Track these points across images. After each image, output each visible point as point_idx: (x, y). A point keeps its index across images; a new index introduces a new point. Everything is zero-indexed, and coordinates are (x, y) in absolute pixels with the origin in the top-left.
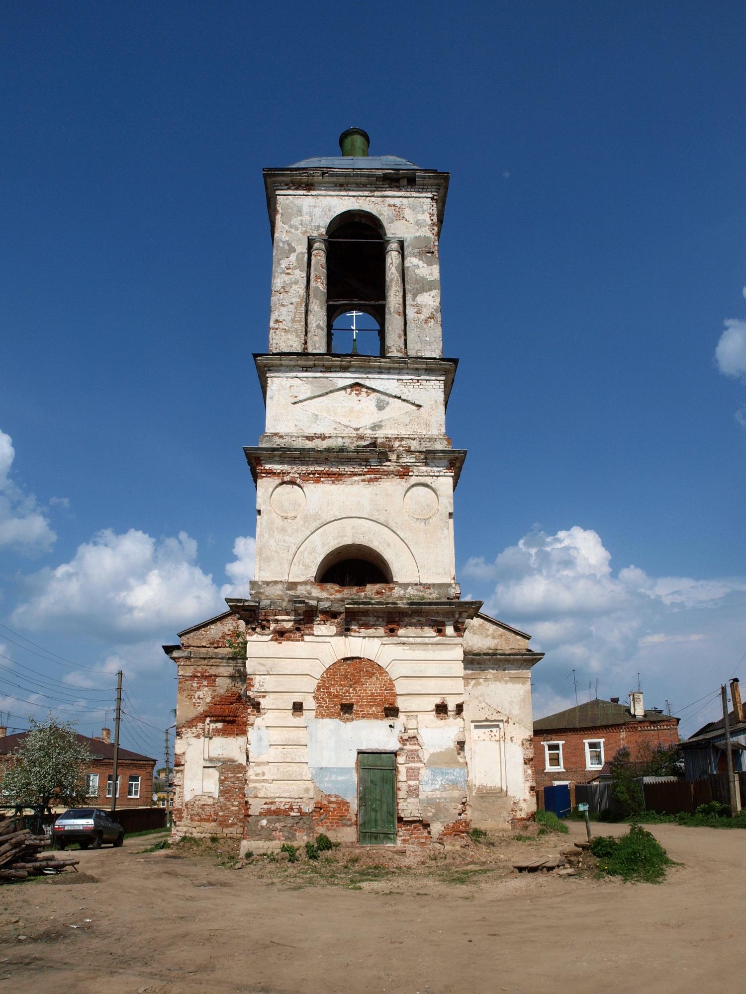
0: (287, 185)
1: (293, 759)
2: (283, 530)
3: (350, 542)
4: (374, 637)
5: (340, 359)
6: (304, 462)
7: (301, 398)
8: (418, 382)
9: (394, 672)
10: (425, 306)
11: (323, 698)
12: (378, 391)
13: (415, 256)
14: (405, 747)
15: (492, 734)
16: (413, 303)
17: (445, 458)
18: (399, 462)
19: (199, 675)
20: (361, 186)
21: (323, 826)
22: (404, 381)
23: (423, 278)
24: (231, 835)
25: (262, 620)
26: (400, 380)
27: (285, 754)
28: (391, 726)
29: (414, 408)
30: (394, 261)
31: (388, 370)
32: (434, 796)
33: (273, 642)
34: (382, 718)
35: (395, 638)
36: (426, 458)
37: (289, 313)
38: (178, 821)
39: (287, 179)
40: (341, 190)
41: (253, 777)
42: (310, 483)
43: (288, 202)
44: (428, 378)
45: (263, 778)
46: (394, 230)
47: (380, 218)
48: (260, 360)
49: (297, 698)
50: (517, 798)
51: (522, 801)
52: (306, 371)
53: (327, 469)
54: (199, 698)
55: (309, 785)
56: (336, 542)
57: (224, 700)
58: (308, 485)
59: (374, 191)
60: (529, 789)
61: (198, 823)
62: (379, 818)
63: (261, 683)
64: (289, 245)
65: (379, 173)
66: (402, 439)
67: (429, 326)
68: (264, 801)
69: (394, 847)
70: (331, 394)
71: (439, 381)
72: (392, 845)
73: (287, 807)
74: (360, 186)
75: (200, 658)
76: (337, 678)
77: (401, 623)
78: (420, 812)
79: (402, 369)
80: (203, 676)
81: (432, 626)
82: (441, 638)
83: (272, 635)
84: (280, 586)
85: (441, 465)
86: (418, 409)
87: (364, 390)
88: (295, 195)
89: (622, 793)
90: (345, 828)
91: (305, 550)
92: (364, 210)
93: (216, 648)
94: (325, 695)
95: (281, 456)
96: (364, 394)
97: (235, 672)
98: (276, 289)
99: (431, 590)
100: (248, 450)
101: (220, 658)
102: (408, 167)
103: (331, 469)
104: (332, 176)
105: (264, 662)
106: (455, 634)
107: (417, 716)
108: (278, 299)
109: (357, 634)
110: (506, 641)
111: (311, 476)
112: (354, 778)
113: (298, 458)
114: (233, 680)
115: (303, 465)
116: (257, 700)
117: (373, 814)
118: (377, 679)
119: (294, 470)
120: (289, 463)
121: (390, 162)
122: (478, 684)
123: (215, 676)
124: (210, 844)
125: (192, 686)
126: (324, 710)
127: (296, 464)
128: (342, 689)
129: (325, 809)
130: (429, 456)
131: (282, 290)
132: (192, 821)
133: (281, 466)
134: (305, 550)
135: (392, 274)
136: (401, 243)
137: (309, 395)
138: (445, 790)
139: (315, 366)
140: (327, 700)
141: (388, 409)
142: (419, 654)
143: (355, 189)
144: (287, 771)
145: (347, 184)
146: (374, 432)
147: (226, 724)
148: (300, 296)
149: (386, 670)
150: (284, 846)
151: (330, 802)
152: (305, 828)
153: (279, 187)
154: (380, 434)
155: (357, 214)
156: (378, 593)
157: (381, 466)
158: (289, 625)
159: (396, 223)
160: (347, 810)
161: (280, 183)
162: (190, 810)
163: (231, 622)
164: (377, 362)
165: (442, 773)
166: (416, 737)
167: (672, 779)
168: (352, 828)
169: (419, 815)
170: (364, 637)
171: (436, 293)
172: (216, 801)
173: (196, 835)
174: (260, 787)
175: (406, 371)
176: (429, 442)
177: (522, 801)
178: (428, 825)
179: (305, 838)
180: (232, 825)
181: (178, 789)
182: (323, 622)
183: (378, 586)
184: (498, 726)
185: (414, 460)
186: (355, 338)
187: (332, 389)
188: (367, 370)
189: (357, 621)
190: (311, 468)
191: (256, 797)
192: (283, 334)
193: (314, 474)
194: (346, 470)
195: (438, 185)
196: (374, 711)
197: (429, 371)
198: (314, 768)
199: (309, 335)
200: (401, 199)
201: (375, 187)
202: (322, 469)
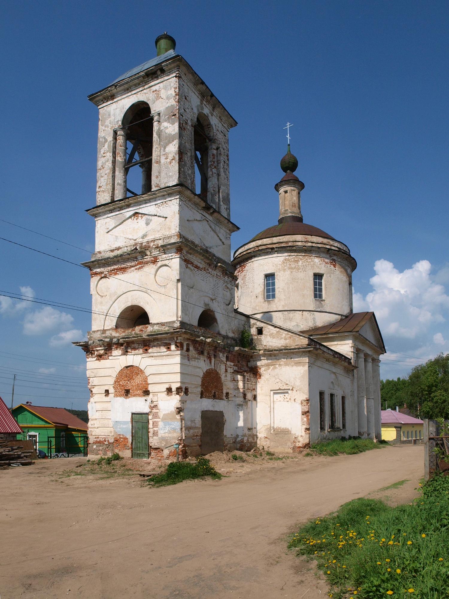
0: (102, 101)
3: (130, 305)
4: (138, 354)
6: (109, 265)
7: (110, 229)
9: (147, 372)
12: (146, 215)
14: (153, 411)
15: (285, 397)
17: (173, 248)
22: (158, 205)
23: (170, 134)
28: (146, 400)
32: (165, 436)
36: (164, 250)
39: (101, 98)
40: (128, 93)
44: (170, 199)
45: (94, 426)
50: (297, 435)
51: (299, 437)
52: (112, 212)
53: (119, 267)
55: (112, 429)
56: (124, 305)
59: (145, 85)
60: (304, 430)
62: (141, 446)
64: (105, 138)
67: (172, 165)
68: (95, 437)
73: (103, 440)
79: (156, 198)
81: (165, 346)
82: (169, 352)
84: (99, 333)
85: (173, 252)
87: (140, 215)
88: (107, 106)
98: (99, 168)
103: (122, 266)
104: (120, 86)
109: (130, 354)
110: (293, 340)
111: (113, 272)
115: (109, 266)
117: (139, 444)
118: (140, 376)
120: (103, 267)
122: (275, 368)
126: (118, 393)
127: (106, 267)
133: (99, 269)
139: (115, 209)
141: (151, 224)
145: (130, 88)
146: (143, 240)
157: (144, 259)
158: (102, 352)
161: (98, 101)
164: (141, 198)
165: (169, 424)
174: (93, 430)
175: (158, 198)
176: (168, 239)
177: (299, 437)
184: (287, 393)
185: (158, 252)
186: (289, 143)
187: (124, 219)
188: (139, 203)
190: (112, 268)
191: (92, 435)
192: (102, 193)
193: (114, 270)
196: (138, 393)
197: (170, 195)
201: (145, 83)
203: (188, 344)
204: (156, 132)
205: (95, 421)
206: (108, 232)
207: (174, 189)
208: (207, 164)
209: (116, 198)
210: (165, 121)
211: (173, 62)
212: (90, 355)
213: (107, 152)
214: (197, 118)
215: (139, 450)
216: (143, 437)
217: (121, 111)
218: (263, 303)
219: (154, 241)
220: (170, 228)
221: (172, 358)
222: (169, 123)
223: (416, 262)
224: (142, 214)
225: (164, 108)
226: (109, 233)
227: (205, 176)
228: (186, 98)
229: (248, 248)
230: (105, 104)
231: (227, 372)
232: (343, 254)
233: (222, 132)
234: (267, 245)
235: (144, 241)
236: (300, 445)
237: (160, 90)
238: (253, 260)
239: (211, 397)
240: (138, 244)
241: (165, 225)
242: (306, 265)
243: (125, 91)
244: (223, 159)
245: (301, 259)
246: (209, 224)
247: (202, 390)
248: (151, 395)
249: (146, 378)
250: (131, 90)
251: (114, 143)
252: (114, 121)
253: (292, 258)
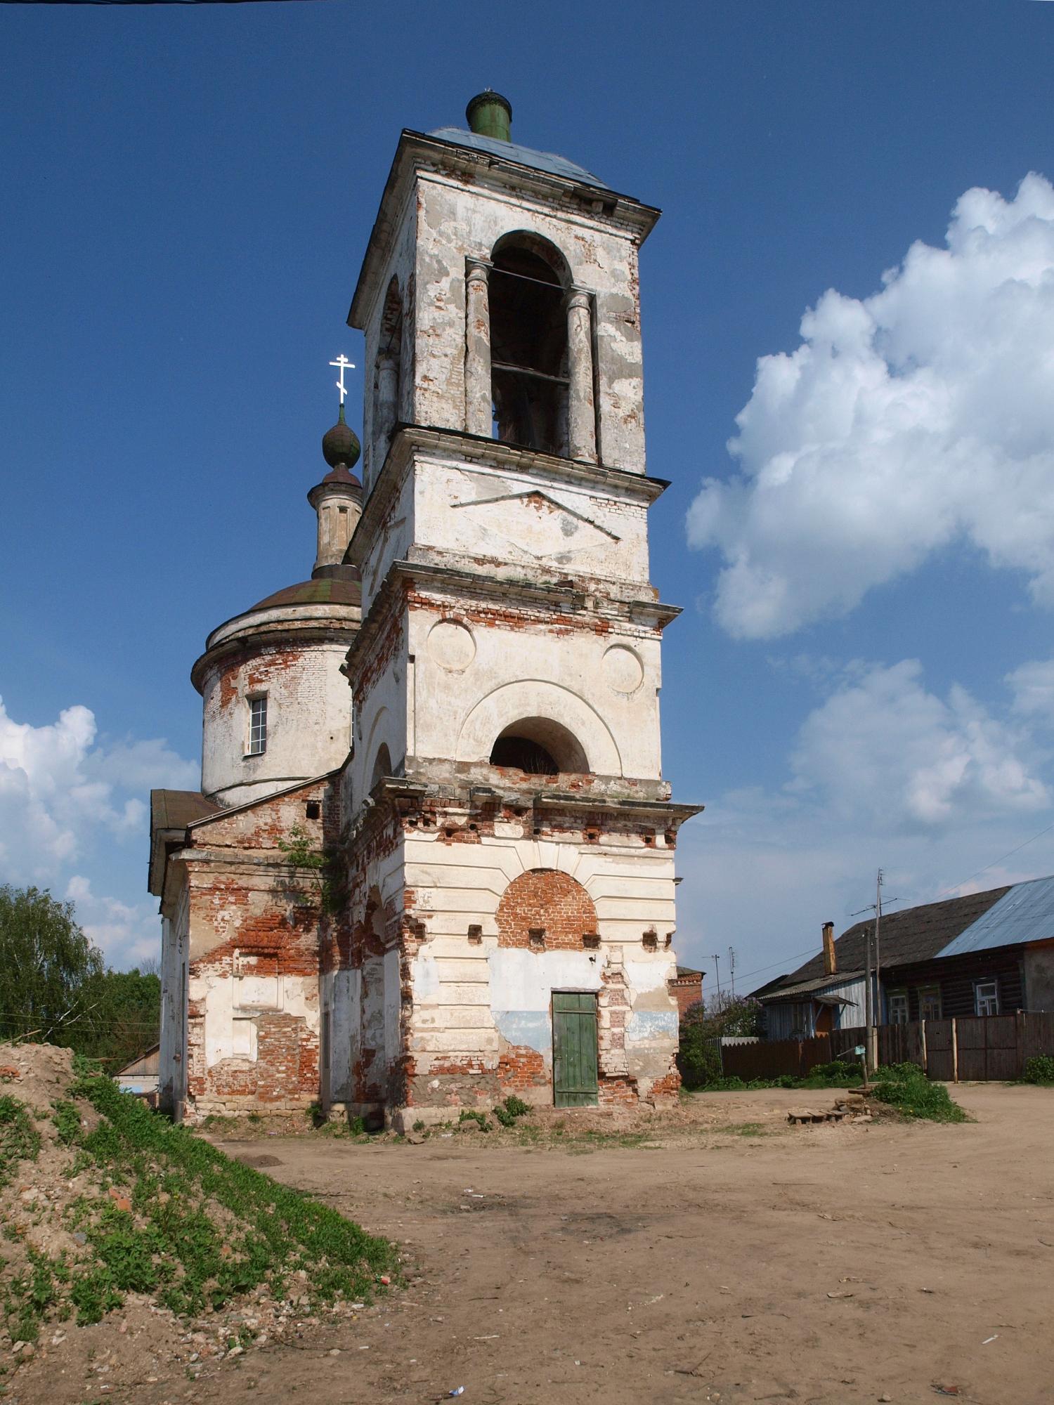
0: (434, 165)
1: (470, 1000)
2: (447, 688)
3: (534, 714)
5: (520, 453)
8: (615, 505)
9: (595, 889)
10: (625, 398)
11: (507, 921)
12: (565, 509)
13: (611, 322)
14: (608, 986)
16: (608, 390)
17: (653, 615)
18: (597, 613)
19: (223, 886)
20: (540, 197)
21: (510, 1086)
23: (621, 358)
24: (278, 1112)
25: (426, 812)
26: (593, 497)
27: (460, 994)
28: (591, 959)
29: (609, 539)
30: (583, 323)
31: (570, 480)
32: (643, 1046)
33: (439, 843)
34: (580, 949)
35: (595, 846)
36: (630, 612)
37: (443, 370)
38: (199, 1095)
39: (436, 156)
40: (511, 196)
41: (419, 1025)
42: (481, 626)
43: (434, 192)
45: (432, 1026)
46: (585, 276)
47: (565, 253)
48: (409, 433)
52: (471, 462)
53: (504, 609)
54: (223, 920)
56: (516, 712)
57: (260, 925)
58: (479, 628)
59: (557, 209)
61: (229, 1097)
62: (578, 1074)
63: (426, 898)
65: (570, 184)
66: (598, 581)
68: (434, 1055)
69: (598, 1109)
70: (502, 502)
71: (642, 507)
72: (595, 1107)
73: (465, 1062)
74: (539, 197)
75: (225, 862)
76: (525, 895)
77: (603, 827)
78: (626, 1065)
79: (596, 482)
80: (227, 889)
82: (649, 849)
83: (438, 834)
84: (447, 766)
86: (616, 543)
87: (546, 503)
88: (445, 185)
89: (696, 1056)
90: (538, 1088)
91: (477, 719)
92: (543, 234)
93: (245, 848)
94: (509, 916)
95: (443, 581)
96: (545, 509)
97: (277, 885)
98: (423, 329)
99: (638, 788)
100: (400, 566)
101: (255, 864)
102: (588, 181)
103: (510, 610)
104: (503, 170)
105: (428, 870)
106: (667, 846)
108: (427, 345)
109: (549, 838)
113: (467, 588)
114: (274, 897)
116: (420, 921)
117: (571, 1069)
118: (574, 898)
119: (460, 605)
120: (453, 593)
121: (555, 164)
123: (246, 889)
124: (249, 1124)
125: (212, 902)
127: (462, 596)
128: (531, 910)
129: (512, 1065)
130: (638, 610)
131: (431, 331)
132: (219, 1094)
133: (442, 596)
134: (477, 719)
135: (581, 341)
136: (592, 299)
137: (473, 498)
138: (655, 1038)
139: (483, 456)
140: (513, 923)
141: (576, 535)
142: (624, 868)
143: (533, 199)
144: (463, 1017)
145: (521, 189)
146: (561, 566)
147: (262, 958)
148: (457, 346)
149: (585, 887)
150: (463, 1113)
151: (518, 1056)
152: (488, 1089)
153: (422, 166)
154: (571, 569)
155: (529, 237)
156: (573, 786)
157: (574, 614)
158: (462, 821)
159: (585, 266)
160: (540, 1065)
161: (426, 159)
162: (215, 1079)
163: (269, 812)
164: (568, 467)
166: (620, 974)
167: (754, 1039)
168: (547, 1087)
169: (624, 1070)
170: (558, 843)
171: (637, 381)
172: (254, 1066)
173: (227, 1114)
174: (429, 1038)
178: (634, 1082)
179: (489, 1101)
180: (278, 1098)
181: (196, 1049)
182: (506, 820)
183: (573, 777)
185: (616, 613)
186: (342, 402)
187: (505, 494)
189: (550, 820)
190: (483, 605)
191: (424, 1051)
192: (435, 399)
193: (486, 613)
194: (529, 613)
195: (642, 224)
196: (570, 940)
197: (630, 492)
198: (498, 1012)
199: (471, 409)
200: (592, 231)
202: (498, 608)
207: (648, 486)
211: (641, 212)
215: (574, 1085)
216: (584, 1051)
221: (657, 865)
223: (70, 706)
229: (308, 614)
238: (325, 647)
241: (616, 554)
243: (505, 187)
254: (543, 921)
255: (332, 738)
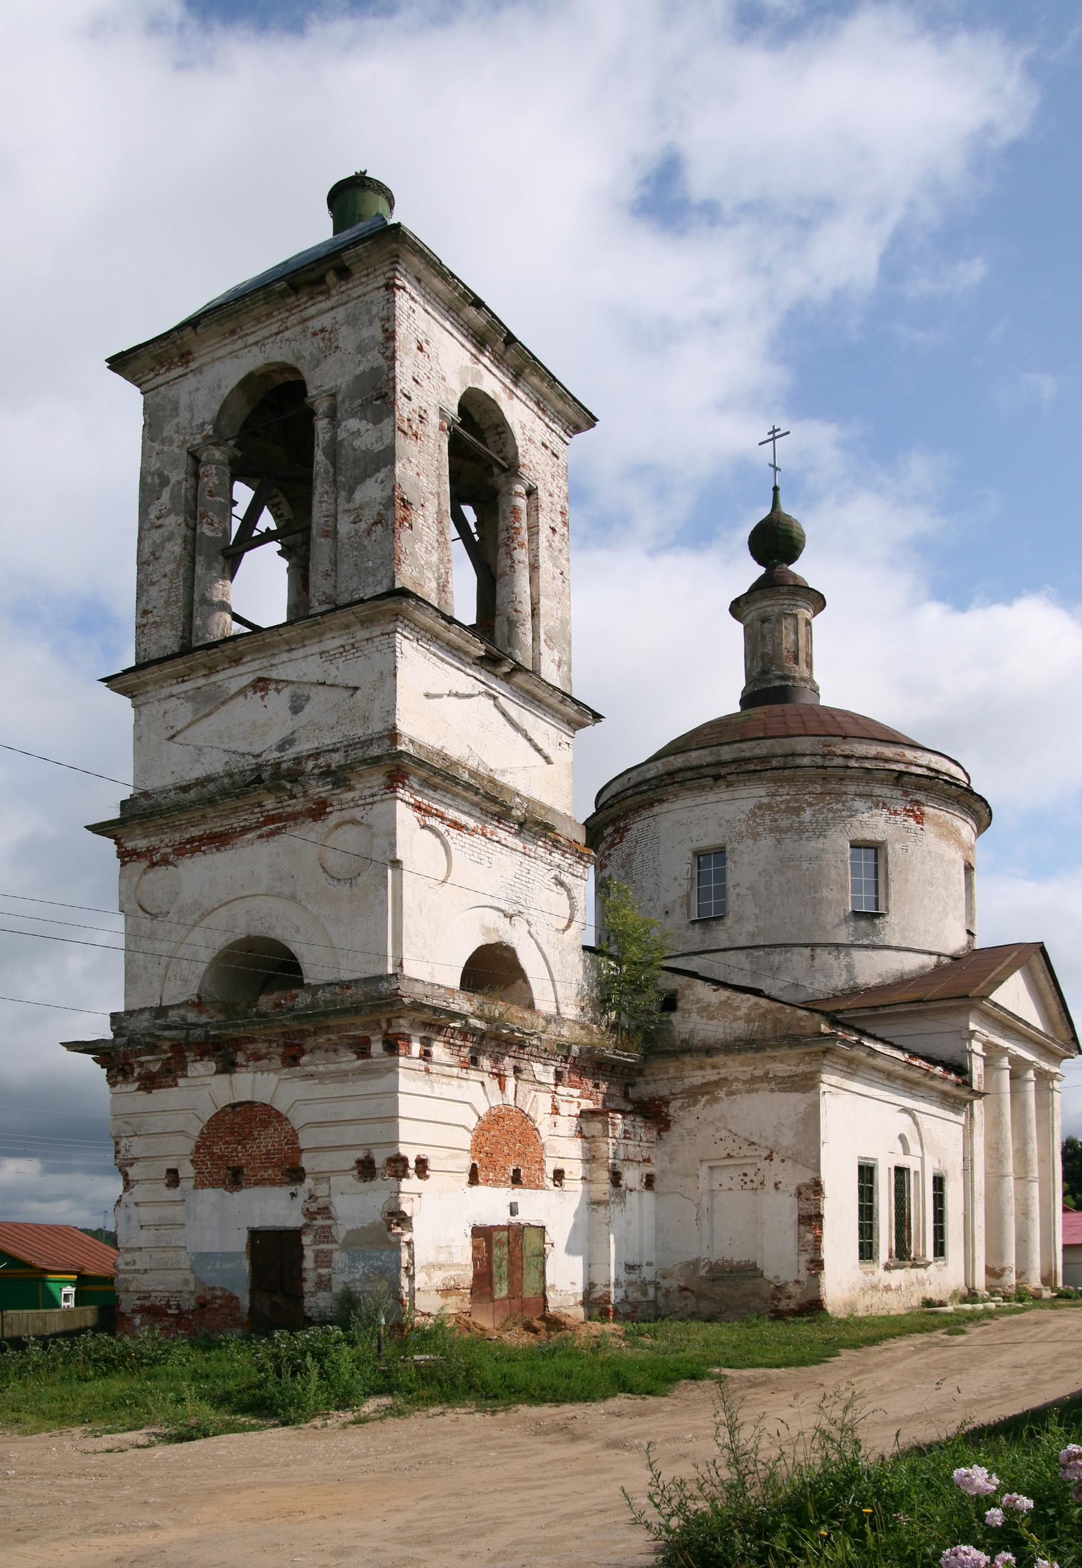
0: (153, 370)
7: (178, 727)
9: (298, 1118)
12: (293, 682)
14: (315, 1223)
15: (747, 1179)
16: (347, 506)
34: (281, 1183)
43: (157, 399)
49: (172, 1165)
52: (183, 681)
67: (374, 538)
73: (163, 1302)
82: (365, 1061)
88: (168, 382)
105: (130, 1120)
107: (329, 1179)
109: (244, 1069)
112: (246, 1265)
118: (276, 1129)
122: (717, 1100)
141: (308, 708)
142: (332, 1089)
146: (283, 754)
151: (215, 1297)
157: (283, 807)
158: (156, 1068)
203: (424, 1037)
204: (324, 449)
205: (138, 1253)
206: (174, 736)
208: (496, 536)
209: (197, 641)
210: (353, 415)
212: (120, 1078)
213: (168, 514)
214: (461, 406)
217: (213, 397)
218: (688, 928)
219: (316, 755)
220: (366, 719)
222: (364, 422)
224: (278, 682)
225: (349, 378)
226: (175, 739)
227: (491, 573)
228: (420, 349)
230: (160, 380)
231: (557, 1113)
232: (946, 787)
233: (544, 444)
234: (702, 767)
235: (285, 758)
236: (792, 1306)
237: (337, 327)
238: (656, 809)
239: (505, 1182)
240: (266, 765)
242: (825, 820)
244: (550, 522)
245: (810, 805)
246: (497, 706)
247: (474, 1166)
248: (309, 1182)
249: (294, 1134)
250: (242, 334)
251: (191, 487)
252: (190, 423)
253: (781, 802)
254: (241, 1158)
255: (667, 912)
